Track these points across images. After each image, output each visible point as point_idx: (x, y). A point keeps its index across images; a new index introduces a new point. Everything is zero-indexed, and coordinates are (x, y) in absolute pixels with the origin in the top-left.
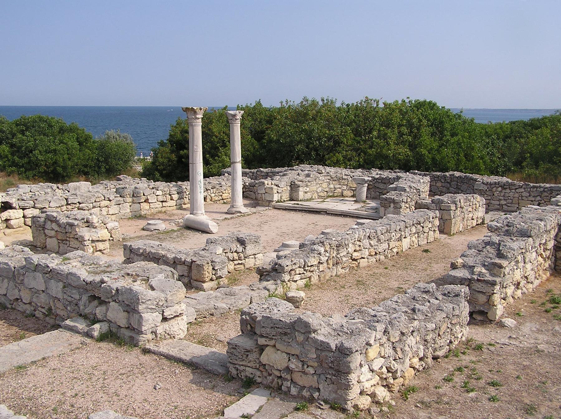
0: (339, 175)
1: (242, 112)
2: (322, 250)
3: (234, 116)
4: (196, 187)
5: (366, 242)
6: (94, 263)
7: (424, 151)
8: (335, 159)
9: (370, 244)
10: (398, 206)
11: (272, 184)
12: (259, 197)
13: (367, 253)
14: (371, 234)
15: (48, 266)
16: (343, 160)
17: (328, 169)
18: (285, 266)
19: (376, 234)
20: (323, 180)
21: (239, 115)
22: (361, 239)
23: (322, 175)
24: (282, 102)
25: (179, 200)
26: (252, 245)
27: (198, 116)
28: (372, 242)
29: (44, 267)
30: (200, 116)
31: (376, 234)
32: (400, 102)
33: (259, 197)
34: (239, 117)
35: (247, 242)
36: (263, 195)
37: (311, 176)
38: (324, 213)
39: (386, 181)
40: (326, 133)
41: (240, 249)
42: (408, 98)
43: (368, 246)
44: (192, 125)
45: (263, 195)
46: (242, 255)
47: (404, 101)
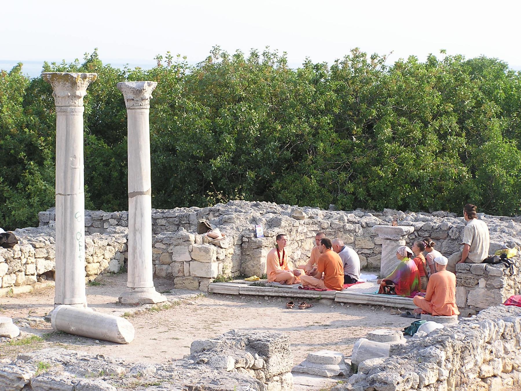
0: (337, 222)
1: (154, 84)
2: (443, 355)
3: (139, 92)
4: (72, 245)
5: (498, 345)
6: (105, 372)
7: (498, 170)
8: (297, 186)
9: (505, 348)
10: (496, 284)
11: (203, 242)
12: (176, 270)
13: (499, 365)
14: (507, 330)
15: (20, 379)
16: (319, 191)
17: (311, 211)
18: (395, 383)
19: (514, 331)
20: (306, 234)
21: (149, 89)
22: (492, 338)
23: (302, 222)
24: (159, 58)
25: (8, 277)
26: (277, 354)
27: (78, 93)
28: (508, 346)
29: (12, 380)
30: (82, 91)
31: (514, 331)
32: (246, 56)
33: (176, 270)
34: (148, 94)
35: (271, 348)
36: (186, 265)
37: (283, 224)
38: (329, 303)
39: (440, 235)
40: (275, 129)
41: (260, 362)
42: (442, 51)
43: (502, 353)
44: (65, 112)
45: (186, 265)
46: (262, 374)
47: (254, 55)
